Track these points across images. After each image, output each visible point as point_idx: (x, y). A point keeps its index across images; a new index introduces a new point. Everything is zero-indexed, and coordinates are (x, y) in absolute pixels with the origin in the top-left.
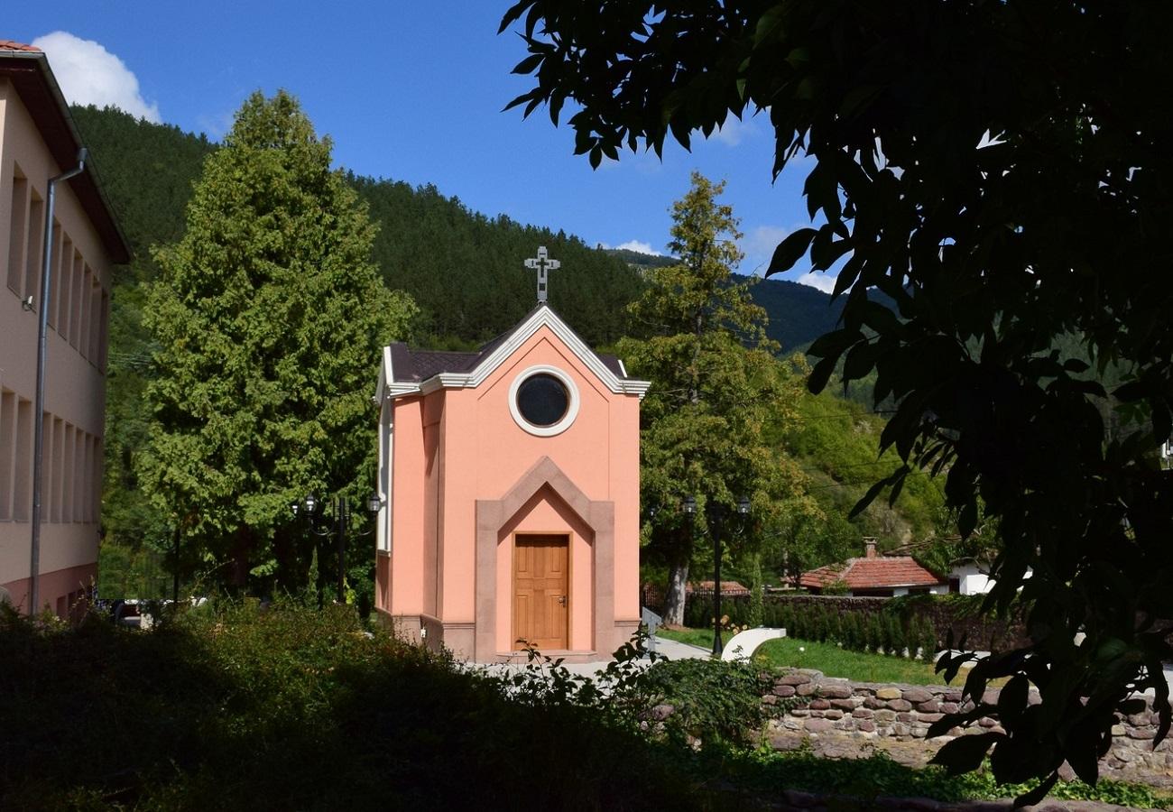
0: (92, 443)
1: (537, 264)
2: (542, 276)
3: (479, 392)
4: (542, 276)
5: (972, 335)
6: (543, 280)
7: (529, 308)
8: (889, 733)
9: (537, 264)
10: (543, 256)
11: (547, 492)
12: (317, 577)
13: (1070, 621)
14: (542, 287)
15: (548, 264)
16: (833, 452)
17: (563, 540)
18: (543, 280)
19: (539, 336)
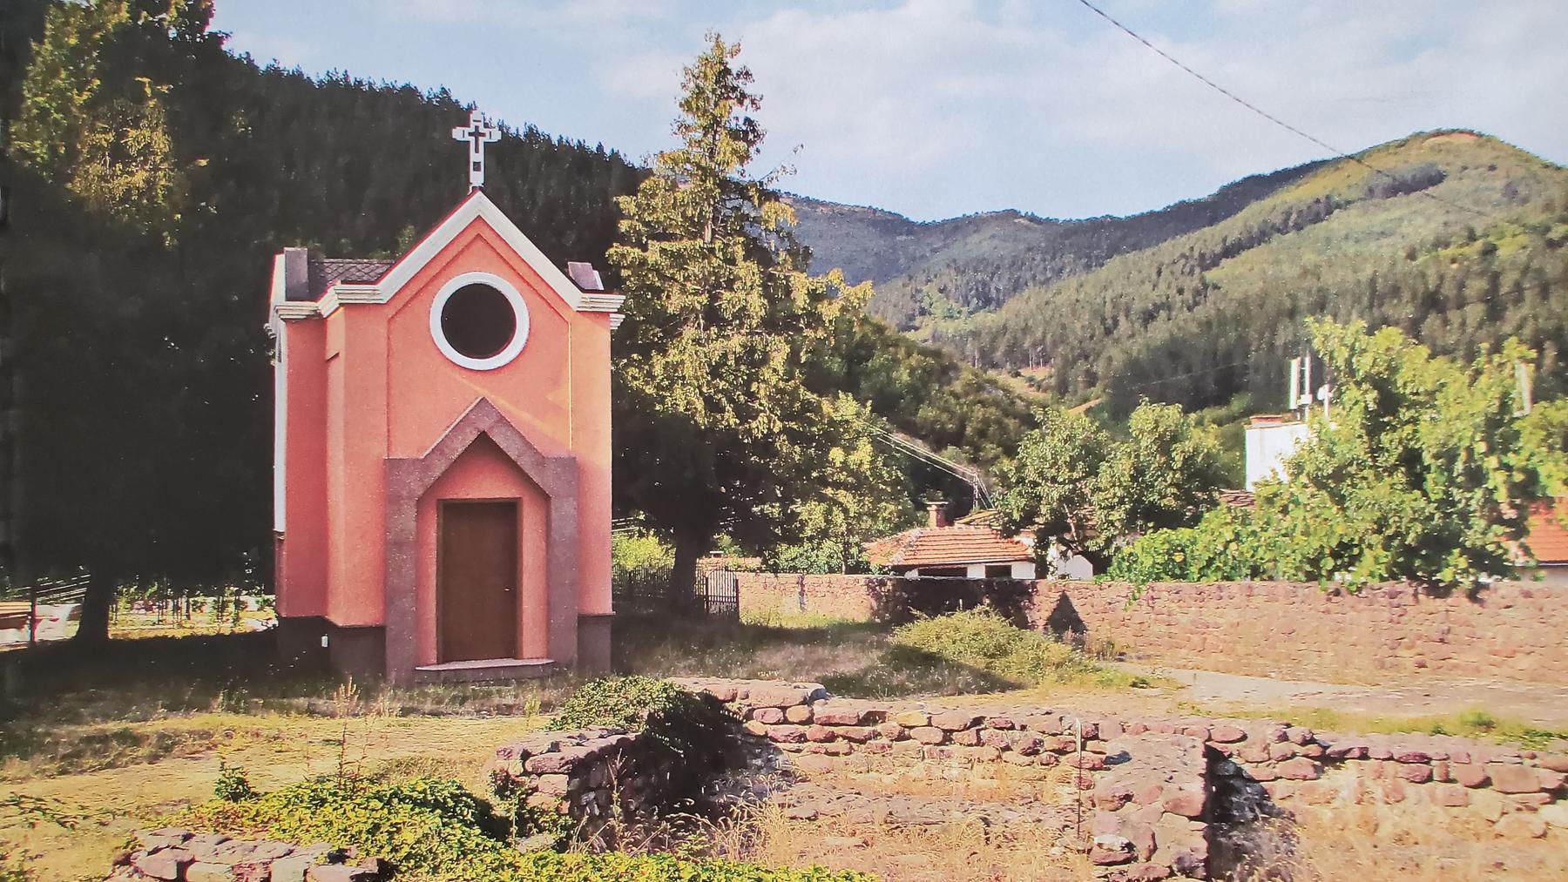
0: (1418, 743)
1: (477, 127)
2: (477, 151)
3: (390, 312)
4: (477, 151)
5: (112, 632)
6: (477, 157)
7: (459, 195)
8: (797, 610)
9: (477, 127)
10: (466, 134)
11: (484, 446)
12: (25, 82)
13: (776, 494)
14: (477, 166)
15: (483, 135)
16: (953, 265)
17: (508, 510)
18: (477, 157)
19: (472, 234)
